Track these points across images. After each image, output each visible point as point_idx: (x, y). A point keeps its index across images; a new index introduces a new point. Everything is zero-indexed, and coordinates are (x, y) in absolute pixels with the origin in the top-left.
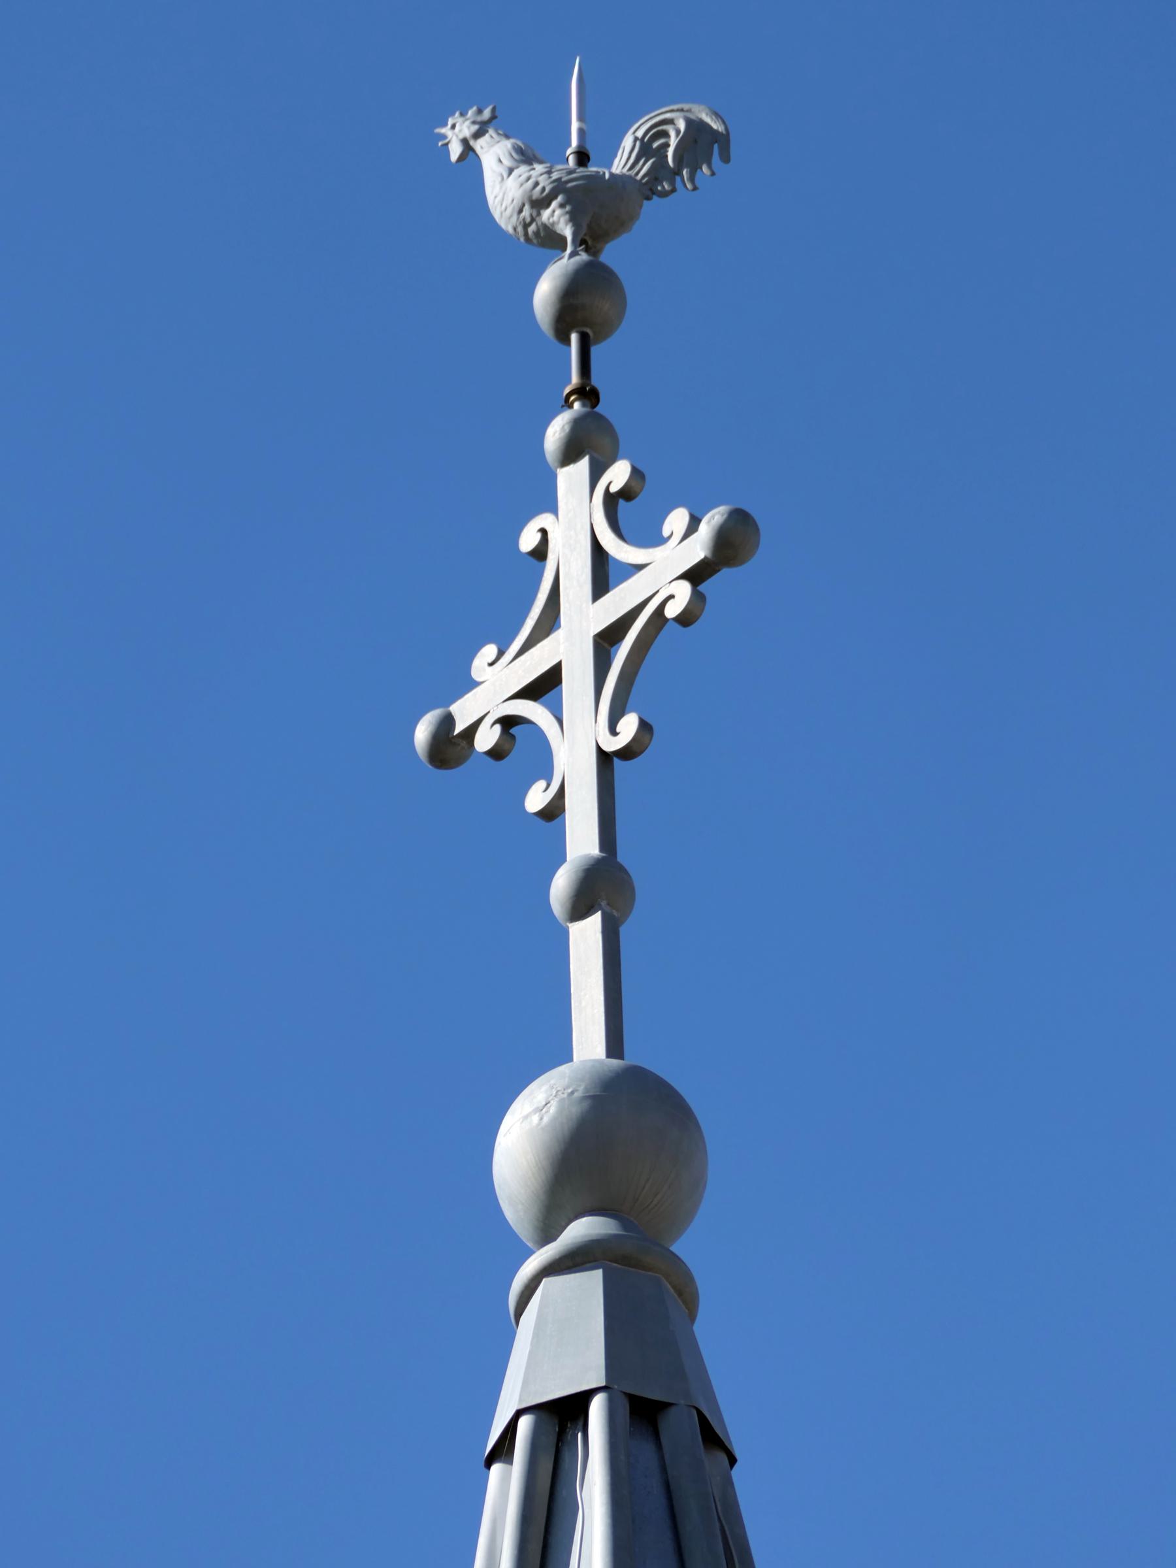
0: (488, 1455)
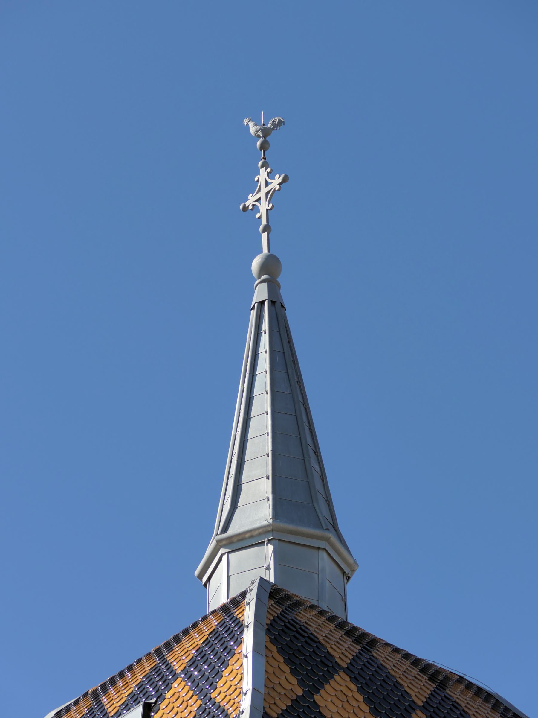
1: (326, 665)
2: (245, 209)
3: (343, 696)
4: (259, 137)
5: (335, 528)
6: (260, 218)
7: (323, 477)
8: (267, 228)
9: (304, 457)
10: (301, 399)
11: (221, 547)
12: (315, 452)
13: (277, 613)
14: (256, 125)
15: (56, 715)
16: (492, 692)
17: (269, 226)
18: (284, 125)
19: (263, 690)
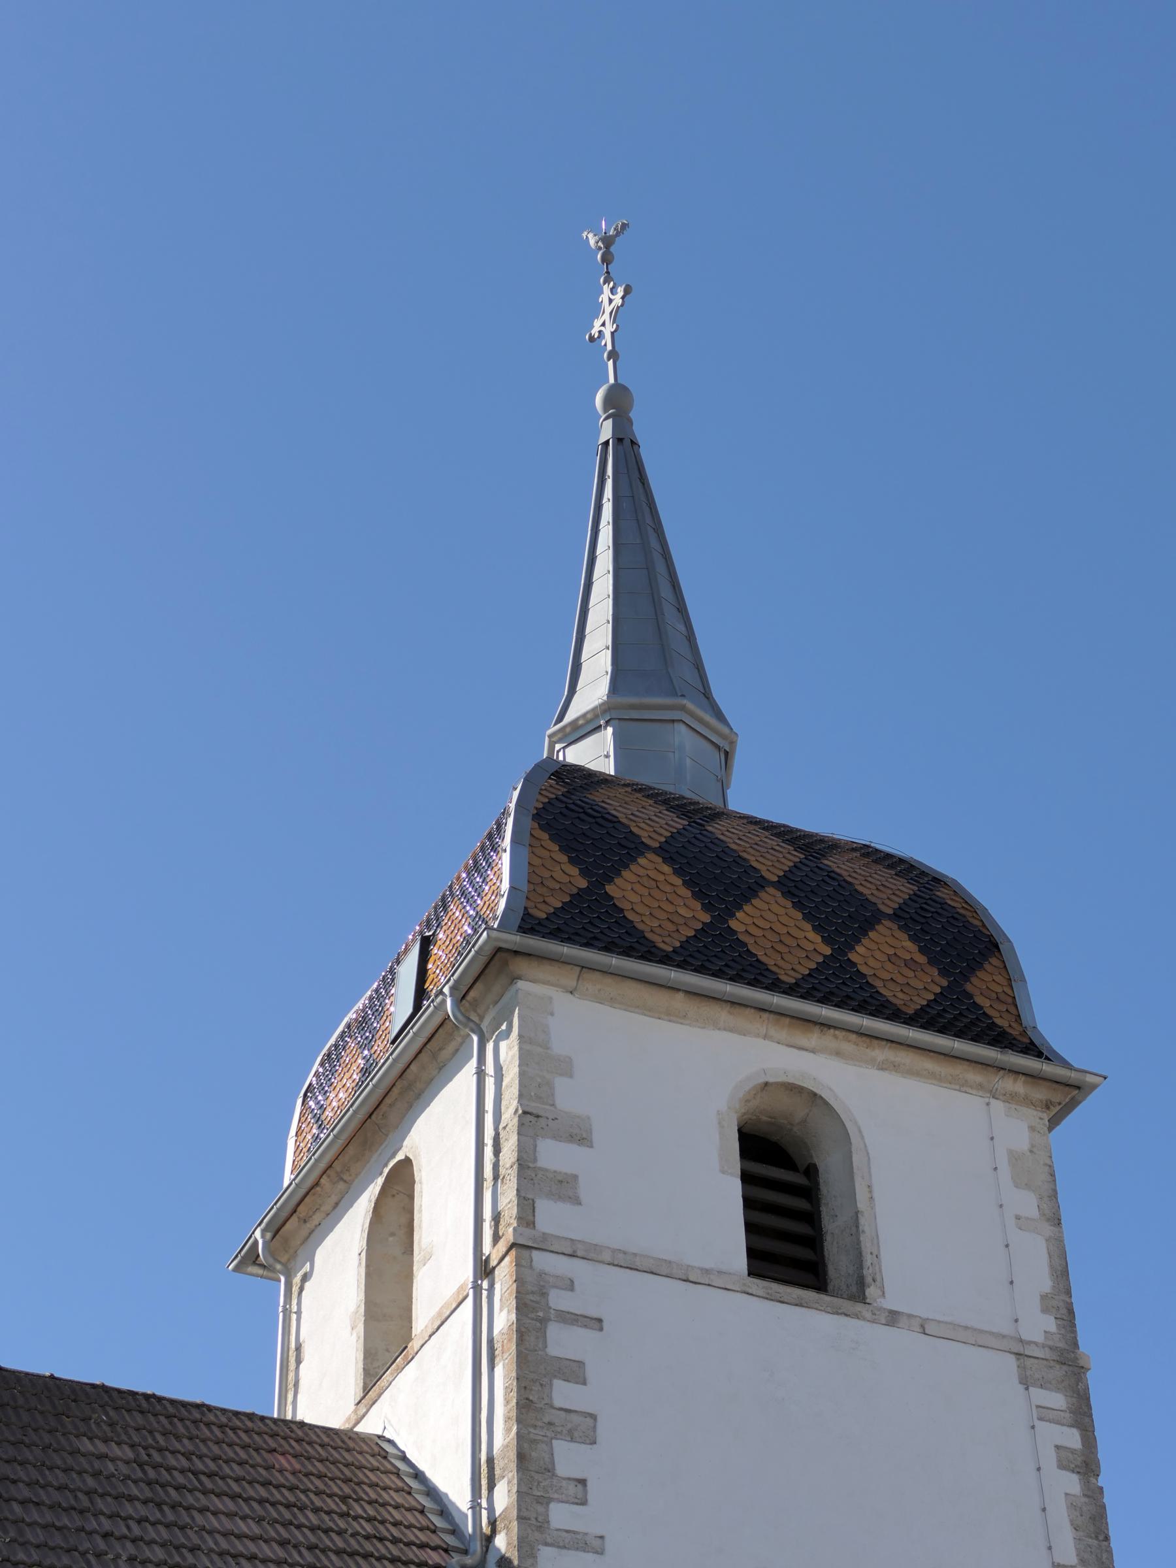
1: (624, 847)
2: (592, 339)
3: (651, 881)
4: (600, 248)
5: (707, 694)
6: (605, 345)
7: (690, 637)
8: (613, 355)
9: (656, 615)
11: (556, 743)
12: (678, 609)
14: (595, 235)
16: (904, 857)
17: (617, 352)
18: (628, 227)
19: (524, 887)
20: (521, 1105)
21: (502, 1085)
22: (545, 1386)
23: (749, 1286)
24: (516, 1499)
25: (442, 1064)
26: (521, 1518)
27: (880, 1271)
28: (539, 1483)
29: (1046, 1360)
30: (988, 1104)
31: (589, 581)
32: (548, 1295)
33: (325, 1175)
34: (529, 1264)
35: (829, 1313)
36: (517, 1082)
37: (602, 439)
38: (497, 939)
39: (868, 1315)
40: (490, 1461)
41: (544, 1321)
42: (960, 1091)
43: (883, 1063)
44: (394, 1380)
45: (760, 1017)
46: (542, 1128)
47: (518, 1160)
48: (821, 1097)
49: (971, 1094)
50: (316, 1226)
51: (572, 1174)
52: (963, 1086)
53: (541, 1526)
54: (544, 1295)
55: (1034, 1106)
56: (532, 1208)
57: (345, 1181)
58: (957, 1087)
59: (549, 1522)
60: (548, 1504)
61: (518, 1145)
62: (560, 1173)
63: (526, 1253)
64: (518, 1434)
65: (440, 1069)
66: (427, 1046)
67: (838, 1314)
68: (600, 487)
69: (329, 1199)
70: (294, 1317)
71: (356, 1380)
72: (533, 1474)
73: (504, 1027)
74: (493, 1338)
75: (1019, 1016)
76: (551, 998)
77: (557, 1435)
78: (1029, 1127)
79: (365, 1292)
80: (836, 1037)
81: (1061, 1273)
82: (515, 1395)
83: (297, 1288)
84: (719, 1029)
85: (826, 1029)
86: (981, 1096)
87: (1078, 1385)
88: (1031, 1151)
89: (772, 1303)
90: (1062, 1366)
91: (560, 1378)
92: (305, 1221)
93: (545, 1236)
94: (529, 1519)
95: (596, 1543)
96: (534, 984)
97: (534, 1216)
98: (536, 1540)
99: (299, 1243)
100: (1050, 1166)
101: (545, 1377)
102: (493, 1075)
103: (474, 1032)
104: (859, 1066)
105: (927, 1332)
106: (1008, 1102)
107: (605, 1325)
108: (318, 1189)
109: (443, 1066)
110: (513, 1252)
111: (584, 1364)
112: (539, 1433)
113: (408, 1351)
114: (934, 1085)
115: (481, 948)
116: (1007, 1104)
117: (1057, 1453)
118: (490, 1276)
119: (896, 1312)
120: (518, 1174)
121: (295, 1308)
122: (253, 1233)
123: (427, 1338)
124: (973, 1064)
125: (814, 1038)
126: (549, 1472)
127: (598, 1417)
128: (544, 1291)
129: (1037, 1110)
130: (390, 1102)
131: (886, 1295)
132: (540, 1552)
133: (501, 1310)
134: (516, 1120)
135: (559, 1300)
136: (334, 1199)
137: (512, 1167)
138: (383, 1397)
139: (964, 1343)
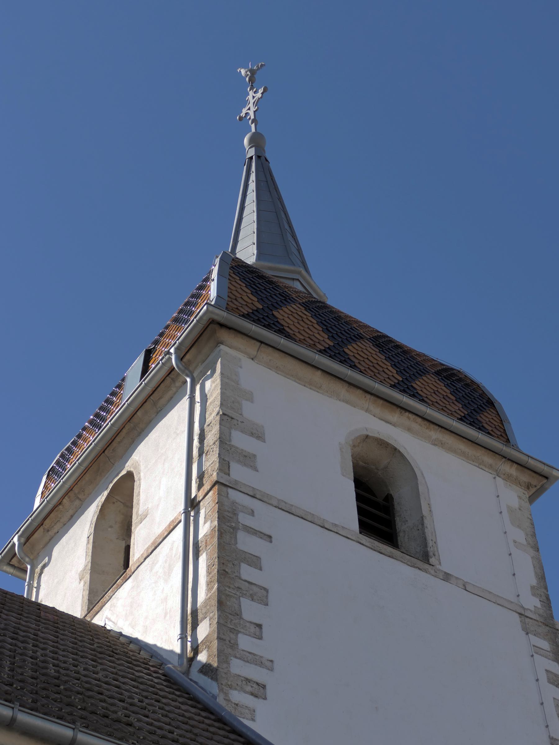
0: (238, 719)
2: (241, 119)
4: (248, 75)
7: (299, 250)
10: (280, 206)
13: (464, 413)
15: (449, 378)
20: (222, 409)
21: (206, 404)
22: (236, 565)
23: (361, 539)
24: (216, 627)
25: (159, 409)
26: (219, 638)
27: (438, 551)
28: (232, 620)
29: (537, 621)
30: (495, 478)
31: (241, 218)
32: (238, 515)
33: (67, 496)
34: (226, 495)
35: (409, 565)
36: (219, 397)
37: (249, 156)
38: (212, 312)
39: (433, 572)
40: (195, 612)
41: (235, 529)
42: (478, 467)
43: (435, 440)
44: (114, 594)
45: (365, 397)
46: (234, 425)
47: (219, 438)
48: (399, 451)
49: (485, 470)
50: (55, 534)
51: (253, 454)
52: (481, 464)
53: (232, 646)
54: (236, 514)
55: (520, 485)
56: (228, 466)
57: (80, 500)
58: (477, 465)
59: (238, 644)
60: (237, 634)
61: (220, 430)
62: (245, 451)
63: (224, 489)
64: (218, 589)
65: (158, 413)
66: (151, 397)
67: (414, 567)
68: (247, 177)
69: (67, 513)
70: (35, 590)
71: (82, 607)
72: (228, 614)
73: (209, 373)
74: (198, 541)
75: (508, 439)
76: (240, 359)
77: (244, 595)
78: (518, 496)
79: (92, 556)
80: (409, 418)
81: (542, 577)
82: (217, 567)
83: (38, 574)
84: (340, 400)
85: (403, 412)
86: (490, 473)
87: (556, 639)
88: (520, 509)
89: (374, 552)
90: (546, 627)
91: (245, 563)
92: (48, 531)
93: (236, 482)
94: (225, 640)
95: (268, 664)
96: (230, 349)
97: (229, 470)
98: (230, 654)
99: (41, 546)
100: (531, 520)
101: (236, 560)
102: (199, 401)
103: (188, 376)
104: (421, 440)
105: (467, 589)
106: (505, 480)
107: (273, 540)
108: (61, 507)
109: (160, 411)
110: (216, 487)
111: (260, 558)
112: (233, 592)
113: (126, 574)
114: (464, 460)
115: (201, 318)
116: (505, 481)
117: (547, 674)
118: (196, 508)
119: (449, 574)
120: (219, 446)
121: (35, 585)
122: (12, 539)
123: (143, 561)
124: (488, 451)
125: (396, 416)
126: (238, 616)
127: (269, 591)
128: (235, 512)
129: (522, 489)
130: (119, 441)
131: (442, 564)
132: (232, 661)
133: (205, 523)
134: (218, 418)
135: (244, 519)
136: (71, 512)
137: (214, 443)
138: (104, 608)
139: (489, 601)
